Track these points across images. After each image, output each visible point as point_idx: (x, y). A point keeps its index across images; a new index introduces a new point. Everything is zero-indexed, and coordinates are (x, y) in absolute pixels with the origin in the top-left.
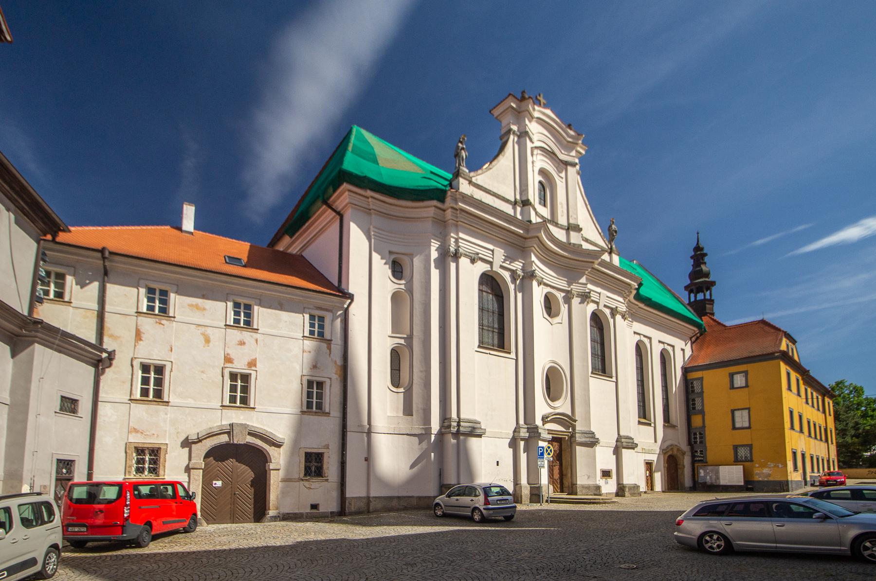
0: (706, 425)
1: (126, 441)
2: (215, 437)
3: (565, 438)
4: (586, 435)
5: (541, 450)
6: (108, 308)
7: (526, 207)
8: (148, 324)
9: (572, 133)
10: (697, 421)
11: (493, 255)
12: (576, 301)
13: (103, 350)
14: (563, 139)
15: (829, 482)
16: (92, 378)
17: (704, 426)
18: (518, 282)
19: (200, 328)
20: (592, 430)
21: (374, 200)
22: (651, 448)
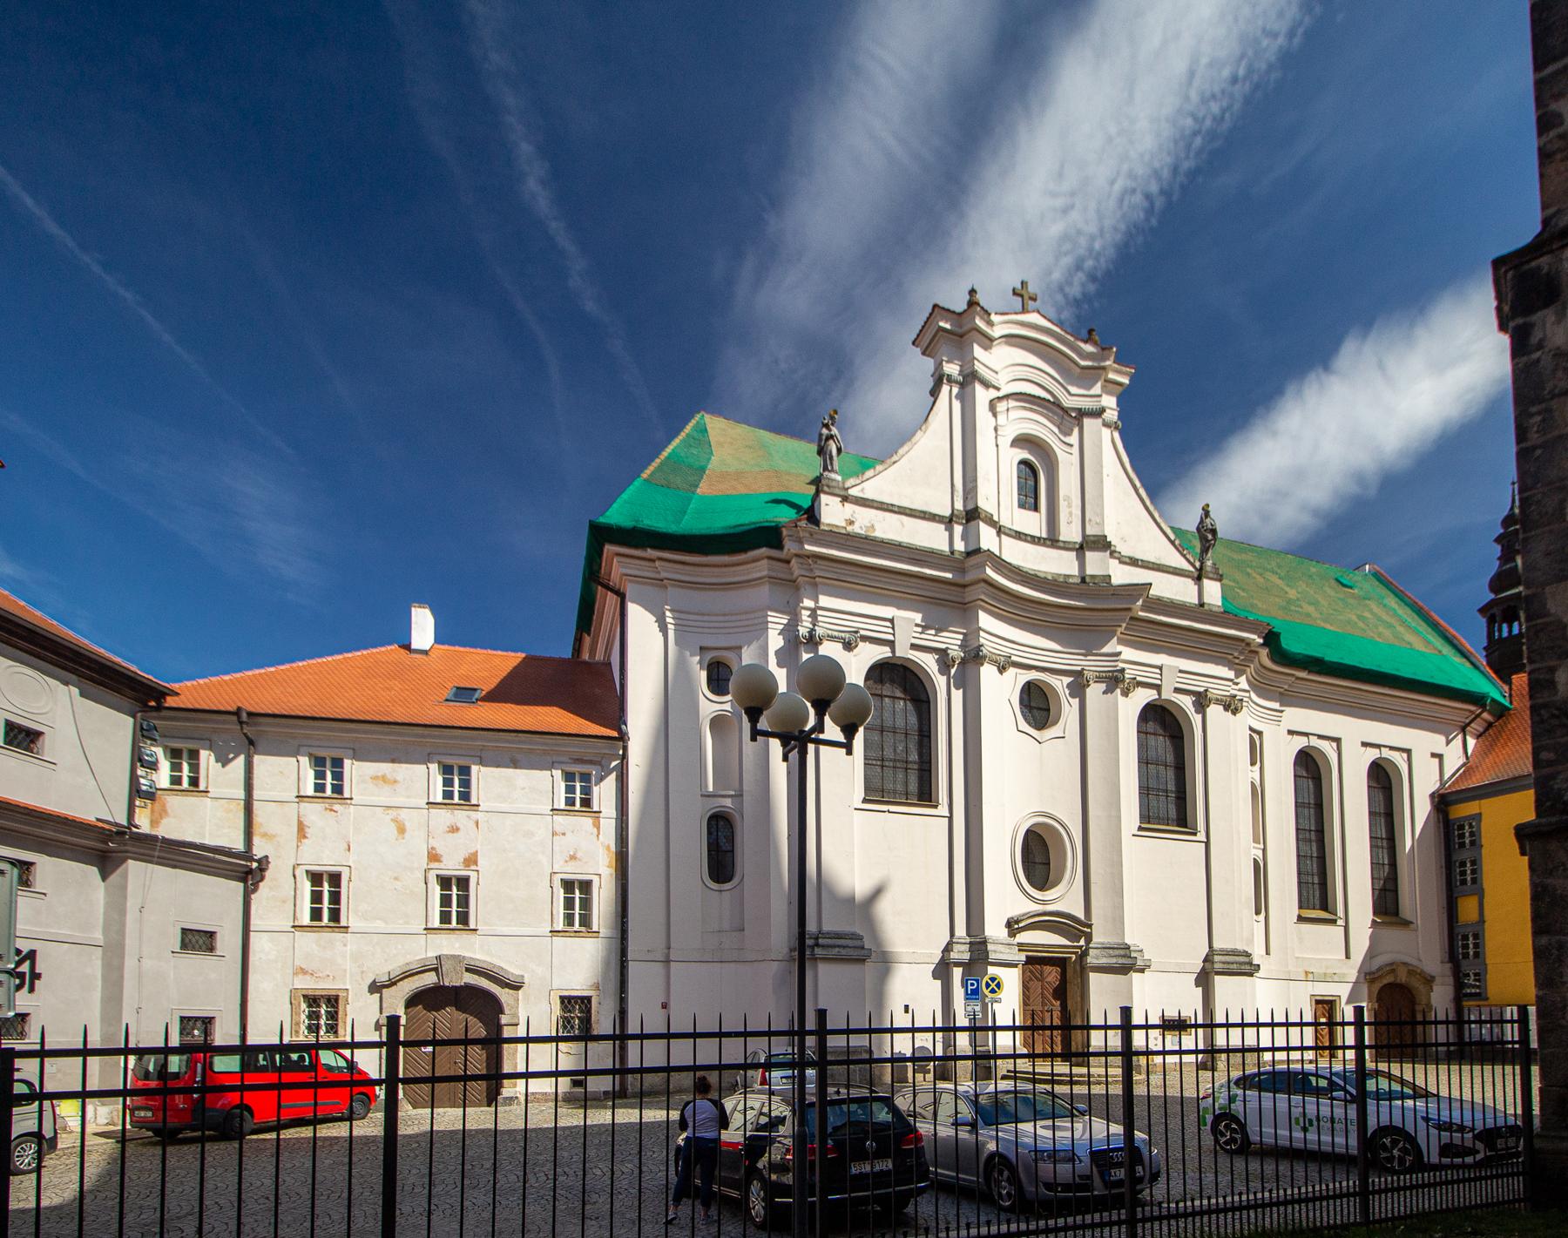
0: (1486, 919)
1: (291, 987)
2: (416, 977)
3: (1070, 958)
4: (1111, 952)
5: (972, 985)
6: (257, 794)
7: (973, 523)
8: (314, 813)
9: (1089, 348)
10: (1468, 909)
11: (893, 628)
12: (1094, 691)
13: (251, 859)
14: (1072, 365)
15: (1534, 1045)
16: (241, 899)
17: (1482, 921)
18: (953, 671)
19: (390, 811)
20: (1126, 941)
21: (663, 563)
22: (1330, 971)
